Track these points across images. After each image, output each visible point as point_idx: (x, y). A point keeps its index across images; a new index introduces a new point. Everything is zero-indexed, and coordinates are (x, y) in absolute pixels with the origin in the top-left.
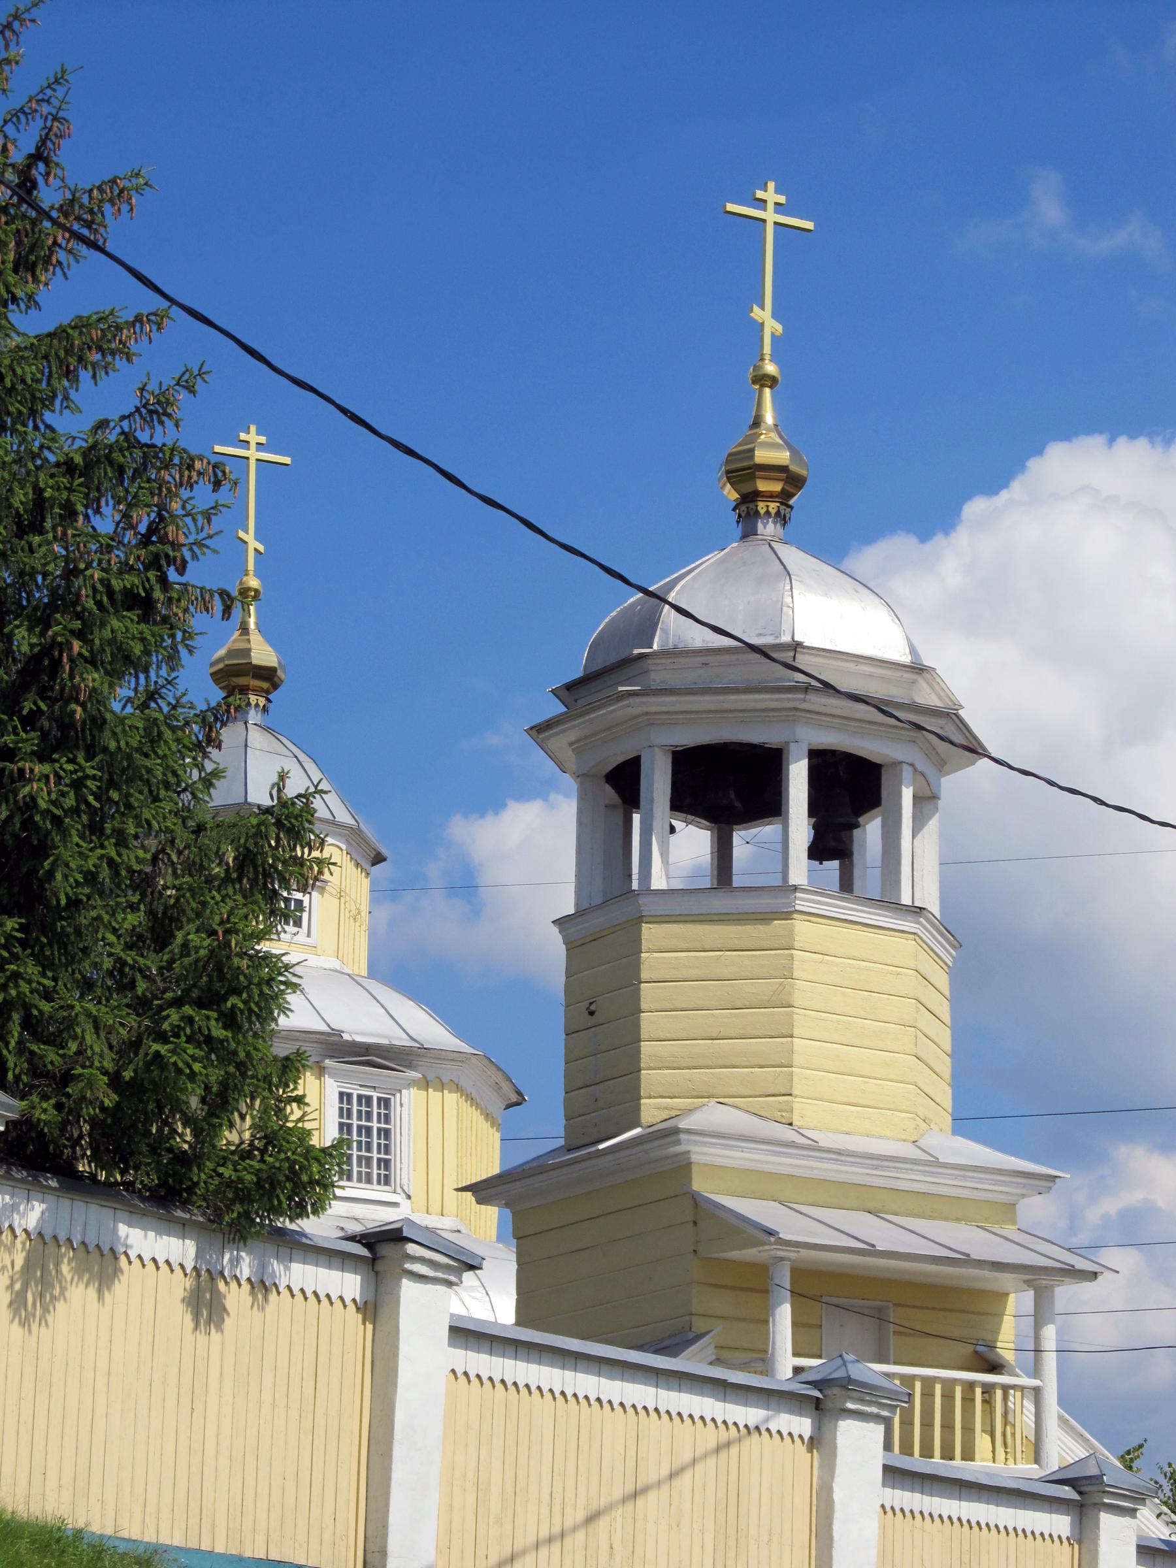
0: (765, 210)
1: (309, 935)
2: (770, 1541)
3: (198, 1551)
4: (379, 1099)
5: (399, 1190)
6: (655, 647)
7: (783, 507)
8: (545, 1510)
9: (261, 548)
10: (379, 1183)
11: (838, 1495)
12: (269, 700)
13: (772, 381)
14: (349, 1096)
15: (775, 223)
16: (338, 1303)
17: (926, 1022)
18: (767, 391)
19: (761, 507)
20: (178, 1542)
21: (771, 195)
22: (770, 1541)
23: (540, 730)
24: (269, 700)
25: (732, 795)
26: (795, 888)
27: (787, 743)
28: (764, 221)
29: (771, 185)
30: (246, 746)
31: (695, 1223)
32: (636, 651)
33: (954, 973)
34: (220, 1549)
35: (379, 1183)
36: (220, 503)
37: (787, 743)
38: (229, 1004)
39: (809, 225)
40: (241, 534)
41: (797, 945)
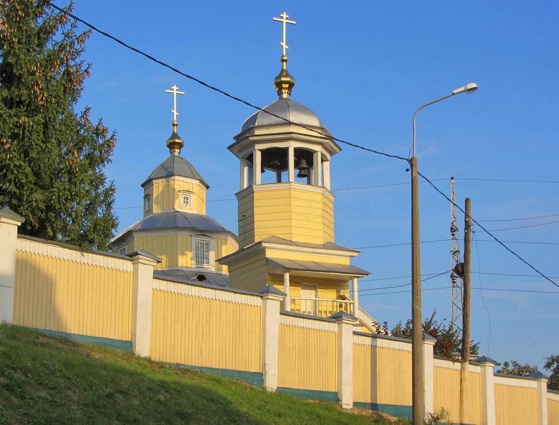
0: (283, 19)
1: (190, 206)
2: (249, 333)
3: (83, 335)
4: (206, 243)
5: (211, 265)
6: (256, 125)
7: (289, 91)
8: (183, 325)
9: (178, 114)
10: (206, 264)
11: (267, 320)
12: (181, 151)
13: (286, 61)
14: (198, 243)
15: (286, 22)
16: (394, 349)
17: (328, 216)
18: (284, 63)
19: (283, 91)
20: (76, 333)
21: (285, 16)
22: (249, 333)
23: (230, 148)
24: (180, 150)
25: (277, 161)
26: (291, 182)
27: (289, 147)
28: (283, 22)
29: (285, 13)
30: (174, 161)
31: (267, 265)
32: (251, 126)
33: (334, 203)
34: (89, 335)
35: (206, 264)
36: (82, 61)
37: (289, 147)
38: (555, 363)
39: (295, 23)
40: (173, 111)
41: (292, 197)
